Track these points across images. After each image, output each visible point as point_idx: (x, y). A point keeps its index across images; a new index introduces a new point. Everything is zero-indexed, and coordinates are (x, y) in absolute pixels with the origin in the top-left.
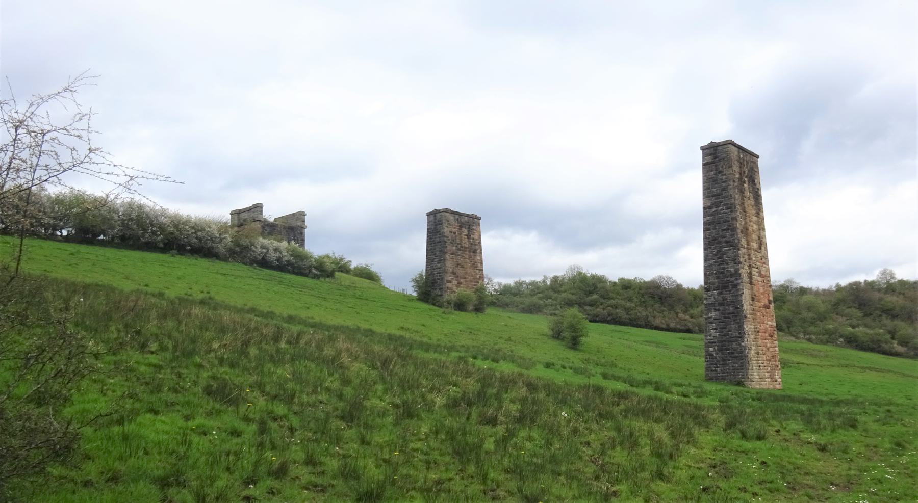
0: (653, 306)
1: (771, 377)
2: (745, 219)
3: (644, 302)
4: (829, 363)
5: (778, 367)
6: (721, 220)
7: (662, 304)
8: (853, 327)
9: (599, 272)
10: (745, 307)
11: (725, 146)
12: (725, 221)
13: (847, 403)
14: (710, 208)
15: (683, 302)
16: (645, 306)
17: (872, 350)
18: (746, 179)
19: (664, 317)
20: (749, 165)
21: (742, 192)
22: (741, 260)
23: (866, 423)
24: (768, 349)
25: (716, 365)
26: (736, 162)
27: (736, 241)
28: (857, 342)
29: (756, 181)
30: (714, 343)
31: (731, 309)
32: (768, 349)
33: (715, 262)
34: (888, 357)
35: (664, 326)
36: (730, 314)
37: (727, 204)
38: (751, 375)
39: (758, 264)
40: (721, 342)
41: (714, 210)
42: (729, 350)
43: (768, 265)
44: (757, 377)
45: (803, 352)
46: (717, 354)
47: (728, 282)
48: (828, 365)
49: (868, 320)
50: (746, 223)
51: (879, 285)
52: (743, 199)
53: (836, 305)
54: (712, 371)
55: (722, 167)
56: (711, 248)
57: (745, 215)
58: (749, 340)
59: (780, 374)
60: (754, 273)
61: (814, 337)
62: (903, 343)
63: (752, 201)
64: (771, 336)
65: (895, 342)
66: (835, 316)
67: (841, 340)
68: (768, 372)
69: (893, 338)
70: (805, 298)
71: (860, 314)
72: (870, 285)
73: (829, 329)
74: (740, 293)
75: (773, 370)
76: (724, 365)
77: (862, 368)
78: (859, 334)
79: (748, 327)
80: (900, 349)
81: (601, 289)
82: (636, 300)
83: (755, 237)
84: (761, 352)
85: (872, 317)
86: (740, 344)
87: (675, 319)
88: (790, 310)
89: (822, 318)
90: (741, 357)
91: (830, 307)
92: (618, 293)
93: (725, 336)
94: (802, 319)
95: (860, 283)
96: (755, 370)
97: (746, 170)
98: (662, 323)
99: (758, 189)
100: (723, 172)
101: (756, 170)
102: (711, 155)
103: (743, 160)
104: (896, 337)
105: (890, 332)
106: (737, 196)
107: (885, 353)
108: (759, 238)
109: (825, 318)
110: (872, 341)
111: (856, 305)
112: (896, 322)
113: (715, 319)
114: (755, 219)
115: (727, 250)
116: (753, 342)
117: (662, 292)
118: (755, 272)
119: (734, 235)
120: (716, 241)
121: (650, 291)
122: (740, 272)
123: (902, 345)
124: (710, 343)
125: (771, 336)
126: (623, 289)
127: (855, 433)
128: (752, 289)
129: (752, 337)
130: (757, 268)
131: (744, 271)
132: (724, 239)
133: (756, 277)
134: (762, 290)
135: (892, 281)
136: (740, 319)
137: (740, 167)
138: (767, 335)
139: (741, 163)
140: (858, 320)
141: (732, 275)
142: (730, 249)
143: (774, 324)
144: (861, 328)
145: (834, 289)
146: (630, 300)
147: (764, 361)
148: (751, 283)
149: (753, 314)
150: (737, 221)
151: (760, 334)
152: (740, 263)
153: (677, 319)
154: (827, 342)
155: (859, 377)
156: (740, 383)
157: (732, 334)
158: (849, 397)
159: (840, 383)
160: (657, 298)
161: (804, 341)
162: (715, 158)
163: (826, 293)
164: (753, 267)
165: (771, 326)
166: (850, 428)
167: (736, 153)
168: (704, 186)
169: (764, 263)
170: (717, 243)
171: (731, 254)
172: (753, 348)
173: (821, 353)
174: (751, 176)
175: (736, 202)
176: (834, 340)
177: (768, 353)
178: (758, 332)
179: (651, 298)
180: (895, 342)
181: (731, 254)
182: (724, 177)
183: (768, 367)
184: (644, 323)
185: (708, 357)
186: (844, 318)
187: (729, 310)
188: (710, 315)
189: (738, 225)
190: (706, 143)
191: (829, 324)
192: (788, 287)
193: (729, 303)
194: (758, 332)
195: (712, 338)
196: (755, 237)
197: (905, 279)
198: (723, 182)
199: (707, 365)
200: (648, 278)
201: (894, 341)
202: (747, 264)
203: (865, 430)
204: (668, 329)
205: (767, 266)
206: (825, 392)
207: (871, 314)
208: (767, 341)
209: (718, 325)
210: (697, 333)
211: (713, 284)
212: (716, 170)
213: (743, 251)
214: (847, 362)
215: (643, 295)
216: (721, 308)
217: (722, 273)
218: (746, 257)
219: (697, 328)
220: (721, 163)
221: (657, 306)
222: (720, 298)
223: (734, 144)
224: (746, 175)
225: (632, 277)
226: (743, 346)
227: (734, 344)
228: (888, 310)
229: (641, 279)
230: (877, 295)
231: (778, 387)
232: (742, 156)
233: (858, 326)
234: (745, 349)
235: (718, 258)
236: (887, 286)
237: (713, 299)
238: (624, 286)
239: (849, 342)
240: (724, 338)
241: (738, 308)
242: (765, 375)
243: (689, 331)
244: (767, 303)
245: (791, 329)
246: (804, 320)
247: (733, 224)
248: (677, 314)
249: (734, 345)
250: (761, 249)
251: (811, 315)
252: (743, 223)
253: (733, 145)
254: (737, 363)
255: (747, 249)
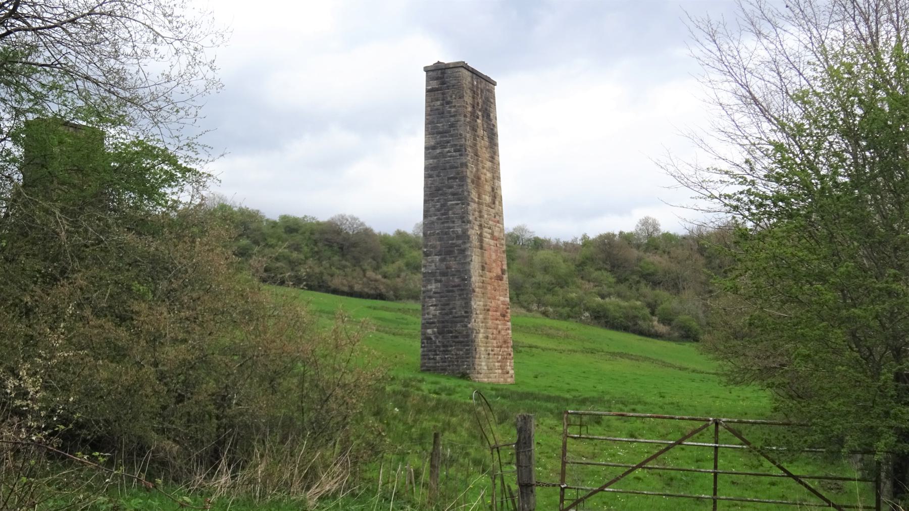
0: (329, 258)
1: (502, 368)
2: (477, 165)
3: (317, 252)
4: (570, 348)
5: (510, 355)
6: (448, 165)
7: (343, 255)
8: (603, 297)
9: (251, 204)
10: (473, 279)
11: (456, 70)
12: (452, 167)
13: (593, 401)
14: (434, 148)
15: (372, 254)
16: (319, 259)
17: (626, 329)
18: (480, 113)
19: (346, 275)
20: (483, 95)
21: (474, 129)
22: (471, 218)
23: (609, 420)
24: (499, 332)
25: (435, 351)
26: (468, 91)
27: (466, 193)
28: (607, 317)
29: (492, 115)
30: (433, 323)
31: (456, 280)
32: (499, 332)
33: (438, 219)
34: (645, 338)
35: (346, 289)
36: (453, 286)
37: (456, 145)
38: (478, 365)
39: (491, 223)
40: (443, 322)
41: (438, 151)
42: (451, 332)
43: (503, 224)
44: (485, 368)
45: (537, 330)
46: (437, 337)
47: (453, 245)
48: (569, 350)
49: (622, 288)
50: (478, 170)
51: (639, 239)
52: (475, 139)
53: (581, 265)
54: (429, 359)
55: (451, 97)
56: (433, 200)
57: (477, 160)
58: (477, 322)
59: (512, 364)
60: (485, 234)
61: (551, 309)
62: (666, 320)
63: (485, 142)
64: (504, 316)
65: (655, 318)
66: (579, 281)
67: (587, 314)
68: (498, 362)
69: (653, 313)
70: (542, 254)
71: (612, 280)
72: (627, 238)
73: (572, 299)
74: (469, 260)
75: (504, 359)
76: (445, 352)
77: (613, 354)
78: (611, 307)
79: (477, 304)
80: (662, 328)
81: (255, 230)
82: (306, 249)
83: (488, 188)
84: (490, 336)
85: (627, 284)
86: (466, 326)
87: (361, 279)
88: (520, 271)
89: (563, 282)
90: (466, 342)
91: (573, 267)
92: (279, 239)
93: (447, 314)
94: (535, 283)
95: (614, 235)
96: (483, 359)
97: (480, 101)
98: (343, 284)
99: (494, 126)
100: (452, 103)
101: (492, 100)
102: (437, 79)
103: (477, 88)
104: (657, 312)
105: (649, 305)
106: (468, 135)
107: (641, 333)
108: (493, 189)
109: (567, 283)
110: (627, 317)
111: (608, 267)
112: (657, 291)
113: (435, 293)
114: (488, 164)
115: (453, 204)
116: (482, 323)
117: (345, 239)
118: (486, 233)
119: (463, 185)
120: (440, 192)
121: (326, 236)
122: (469, 233)
123: (664, 324)
124: (428, 323)
125: (504, 316)
126: (286, 232)
127: (600, 428)
128: (482, 255)
129: (481, 316)
130: (490, 228)
131: (473, 232)
132: (450, 190)
133: (487, 240)
134: (494, 257)
135: (656, 234)
136: (467, 294)
137: (473, 98)
138: (499, 314)
139: (474, 92)
140: (610, 287)
141: (458, 237)
142: (458, 204)
143: (508, 299)
144: (613, 299)
145: (580, 242)
146: (297, 248)
147: (494, 347)
148: (481, 248)
149: (483, 287)
150: (467, 166)
151: (490, 313)
152: (469, 222)
153: (365, 280)
154: (568, 317)
155: (607, 367)
156: (464, 376)
157: (456, 313)
158: (595, 394)
159: (583, 375)
160: (336, 248)
161: (539, 315)
162: (443, 83)
163: (570, 247)
164: (485, 227)
165: (503, 303)
166: (595, 425)
167: (469, 79)
168: (426, 119)
169: (498, 222)
170: (441, 195)
171: (458, 210)
172: (482, 331)
173: (561, 333)
174: (486, 109)
175: (467, 143)
176: (576, 313)
177: (499, 337)
178: (488, 310)
179: (327, 248)
180: (655, 318)
181: (458, 210)
182: (453, 110)
183: (498, 355)
184: (316, 283)
185: (425, 341)
186: (592, 284)
187: (453, 281)
188: (429, 287)
189: (468, 173)
190: (430, 63)
191: (571, 292)
192: (518, 237)
193: (454, 273)
194: (488, 310)
195: (431, 316)
196: (488, 188)
197: (672, 232)
198: (451, 116)
199: (423, 351)
200: (323, 216)
201: (654, 318)
202: (478, 223)
203: (608, 426)
204: (352, 294)
205: (501, 226)
206: (566, 387)
207: (626, 280)
208: (498, 322)
209: (440, 301)
210: (392, 300)
211: (434, 247)
212: (443, 100)
213: (473, 206)
214: (592, 346)
215: (316, 243)
216: (443, 279)
217: (446, 233)
218: (477, 214)
219: (392, 293)
220: (450, 91)
221: (336, 258)
222: (443, 266)
223: (467, 68)
224: (480, 107)
225: (300, 215)
226: (470, 329)
227: (459, 325)
228: (649, 274)
229: (313, 219)
230: (635, 253)
231: (509, 380)
232: (475, 83)
233: (609, 295)
234: (472, 332)
235: (443, 214)
236: (649, 241)
237: (433, 267)
238: (288, 227)
239: (596, 318)
240: (447, 318)
241: (466, 280)
242: (494, 365)
243: (381, 297)
244: (500, 273)
245: (522, 298)
246: (539, 285)
247: (462, 172)
248: (364, 271)
249: (459, 327)
250: (494, 203)
251: (548, 278)
252: (475, 169)
253: (465, 68)
254: (461, 350)
255: (479, 203)
